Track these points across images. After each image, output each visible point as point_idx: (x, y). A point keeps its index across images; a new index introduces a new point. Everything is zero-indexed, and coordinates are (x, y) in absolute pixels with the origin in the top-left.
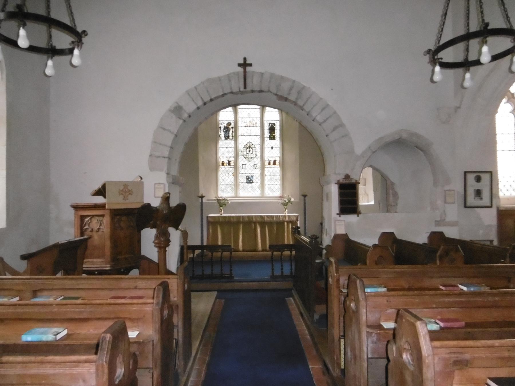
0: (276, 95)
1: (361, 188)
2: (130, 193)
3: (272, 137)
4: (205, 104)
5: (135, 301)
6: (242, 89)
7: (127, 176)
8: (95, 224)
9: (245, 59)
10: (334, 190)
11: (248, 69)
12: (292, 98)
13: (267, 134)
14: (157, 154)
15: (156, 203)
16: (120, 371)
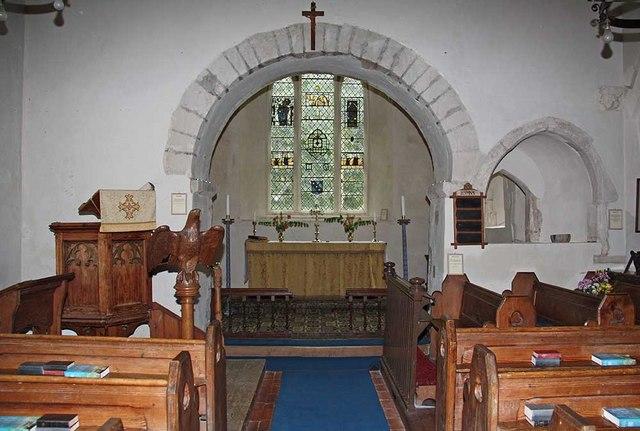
0: (360, 59)
1: (486, 207)
2: (136, 207)
3: (352, 123)
4: (251, 72)
5: (139, 382)
6: (308, 49)
7: (131, 181)
8: (83, 254)
9: (313, 5)
10: (449, 208)
11: (318, 19)
12: (385, 64)
13: (344, 118)
14: (177, 149)
15: (177, 225)
16: (186, 400)
